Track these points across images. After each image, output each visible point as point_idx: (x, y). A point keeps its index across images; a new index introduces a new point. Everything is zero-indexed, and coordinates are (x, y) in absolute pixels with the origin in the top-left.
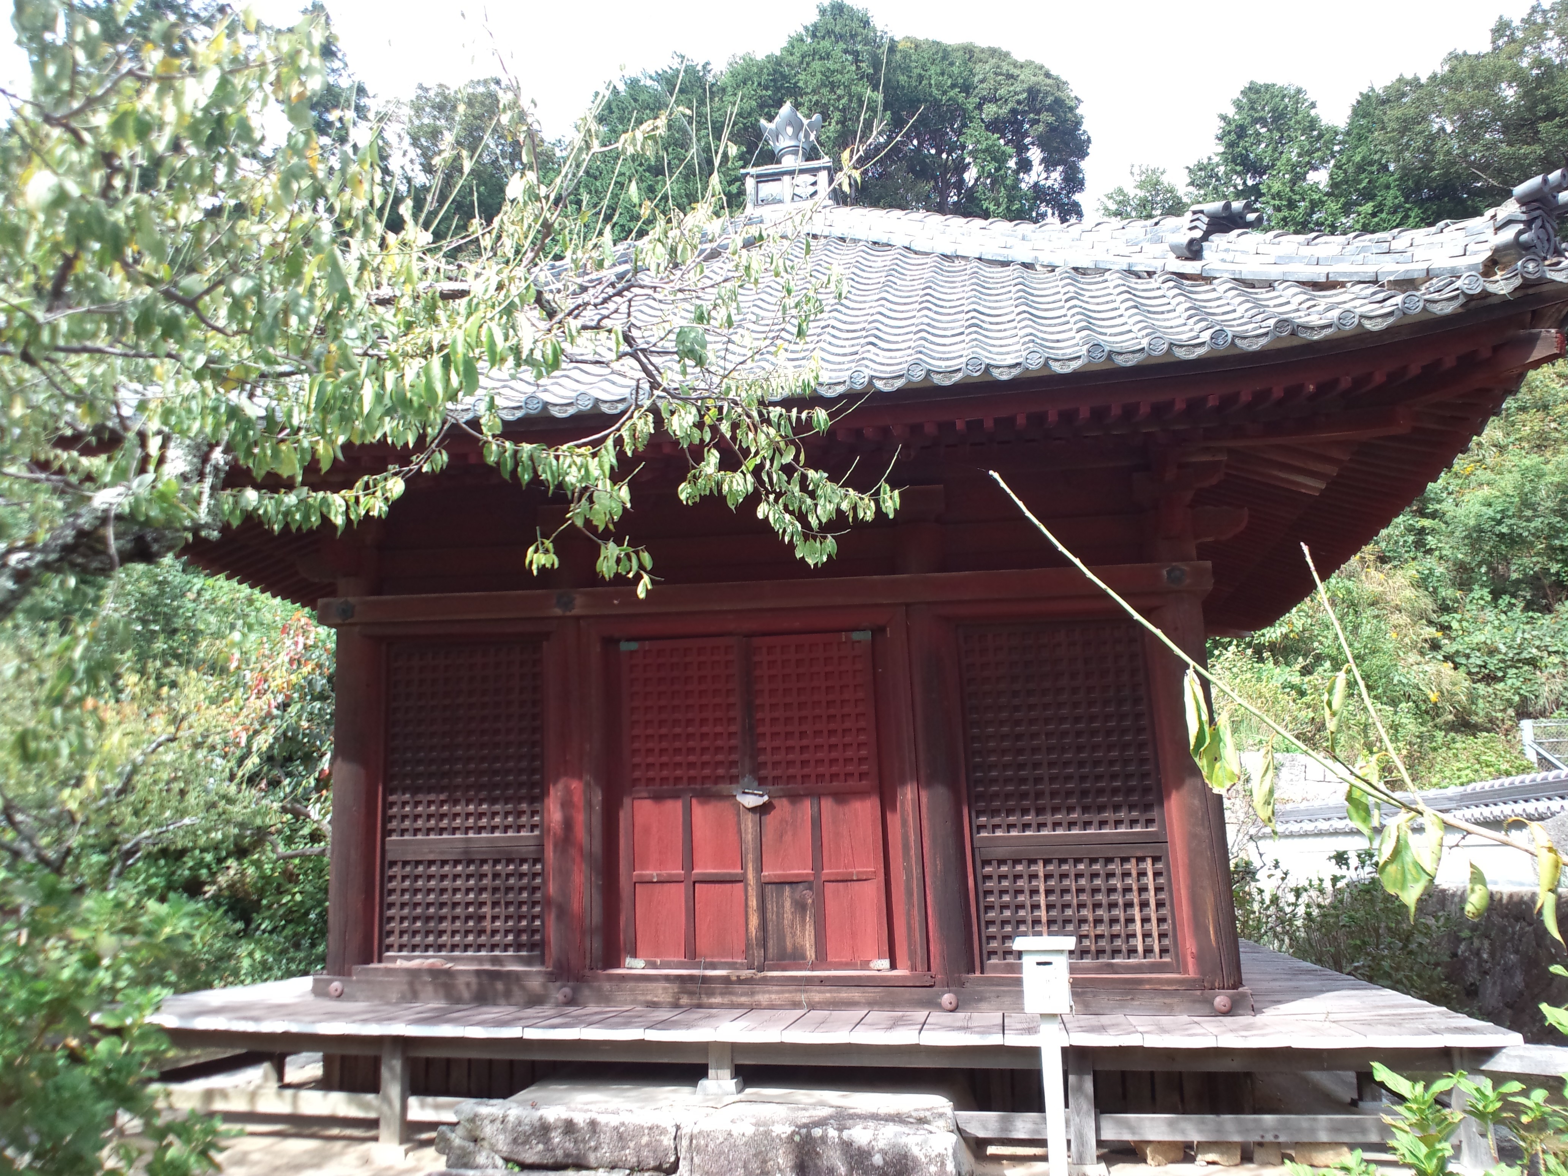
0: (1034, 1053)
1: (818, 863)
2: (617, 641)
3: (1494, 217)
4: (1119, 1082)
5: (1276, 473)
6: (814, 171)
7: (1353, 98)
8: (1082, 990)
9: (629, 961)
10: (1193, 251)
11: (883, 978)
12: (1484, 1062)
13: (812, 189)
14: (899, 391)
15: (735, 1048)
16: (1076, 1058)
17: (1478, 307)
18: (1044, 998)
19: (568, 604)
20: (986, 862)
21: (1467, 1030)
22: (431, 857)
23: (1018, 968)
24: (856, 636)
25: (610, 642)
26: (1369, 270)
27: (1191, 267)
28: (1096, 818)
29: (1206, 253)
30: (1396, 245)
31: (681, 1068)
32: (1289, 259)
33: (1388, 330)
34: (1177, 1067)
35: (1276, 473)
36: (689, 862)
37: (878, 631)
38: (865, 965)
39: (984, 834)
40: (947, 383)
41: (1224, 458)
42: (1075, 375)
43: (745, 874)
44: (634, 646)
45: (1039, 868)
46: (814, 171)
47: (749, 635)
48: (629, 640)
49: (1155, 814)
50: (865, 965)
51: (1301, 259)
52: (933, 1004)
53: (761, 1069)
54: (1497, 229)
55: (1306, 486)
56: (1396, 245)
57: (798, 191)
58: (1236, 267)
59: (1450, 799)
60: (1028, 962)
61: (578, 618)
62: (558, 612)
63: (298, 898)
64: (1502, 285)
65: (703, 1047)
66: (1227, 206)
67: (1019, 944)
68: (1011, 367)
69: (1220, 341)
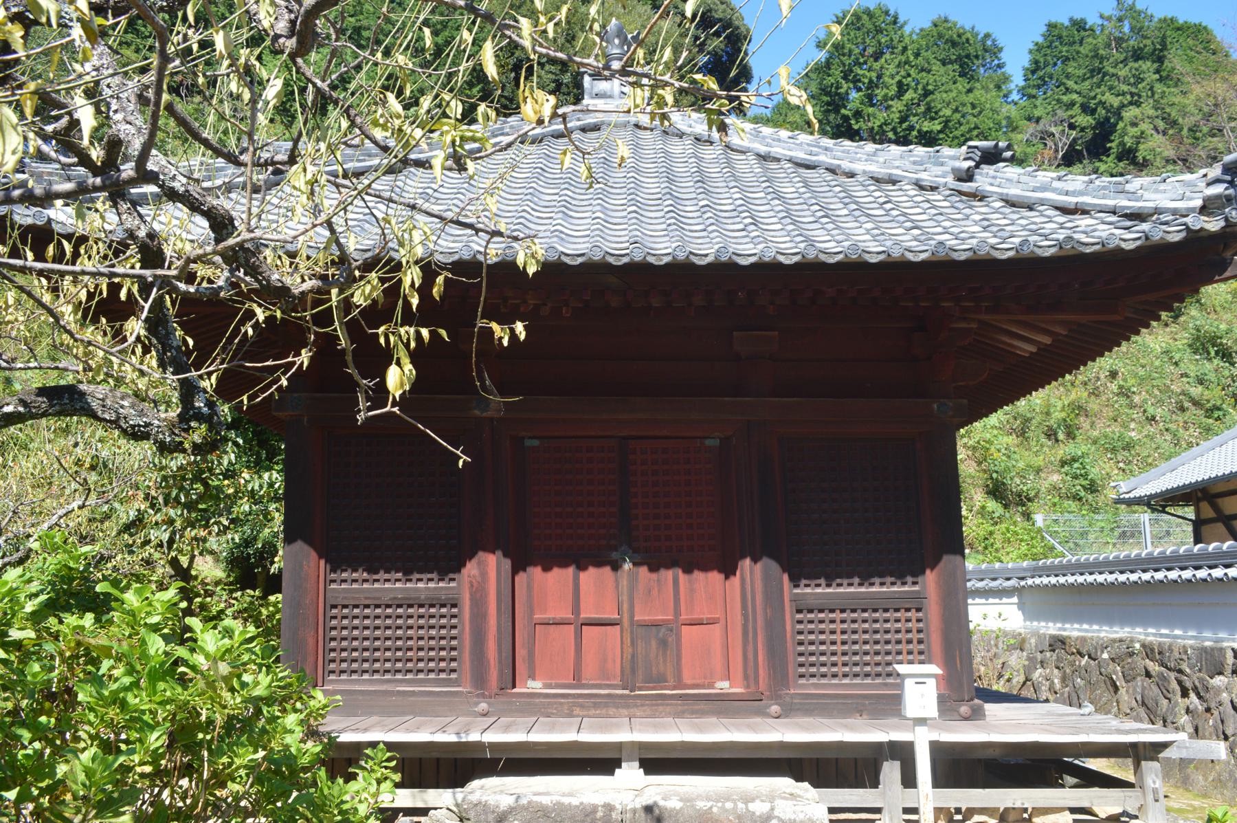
1: (677, 612)
3: (1205, 176)
4: (959, 767)
8: (947, 705)
9: (531, 683)
10: (968, 176)
11: (728, 694)
12: (1160, 752)
14: (796, 264)
16: (938, 749)
17: (1195, 238)
18: (920, 709)
20: (334, 607)
22: (367, 602)
23: (900, 686)
24: (708, 442)
26: (1110, 203)
27: (966, 187)
28: (813, 583)
29: (977, 177)
30: (1128, 187)
31: (600, 762)
32: (1044, 188)
33: (1138, 248)
36: (576, 609)
38: (711, 686)
39: (333, 586)
40: (831, 261)
41: (974, 326)
42: (923, 263)
43: (621, 619)
44: (536, 443)
47: (624, 438)
49: (920, 579)
50: (711, 686)
51: (1054, 190)
52: (763, 713)
53: (659, 762)
54: (1209, 184)
55: (1020, 349)
56: (1128, 187)
58: (1005, 191)
59: (1025, 570)
60: (909, 684)
62: (477, 412)
64: (1214, 225)
65: (619, 746)
66: (997, 145)
67: (902, 669)
68: (879, 253)
69: (1025, 248)
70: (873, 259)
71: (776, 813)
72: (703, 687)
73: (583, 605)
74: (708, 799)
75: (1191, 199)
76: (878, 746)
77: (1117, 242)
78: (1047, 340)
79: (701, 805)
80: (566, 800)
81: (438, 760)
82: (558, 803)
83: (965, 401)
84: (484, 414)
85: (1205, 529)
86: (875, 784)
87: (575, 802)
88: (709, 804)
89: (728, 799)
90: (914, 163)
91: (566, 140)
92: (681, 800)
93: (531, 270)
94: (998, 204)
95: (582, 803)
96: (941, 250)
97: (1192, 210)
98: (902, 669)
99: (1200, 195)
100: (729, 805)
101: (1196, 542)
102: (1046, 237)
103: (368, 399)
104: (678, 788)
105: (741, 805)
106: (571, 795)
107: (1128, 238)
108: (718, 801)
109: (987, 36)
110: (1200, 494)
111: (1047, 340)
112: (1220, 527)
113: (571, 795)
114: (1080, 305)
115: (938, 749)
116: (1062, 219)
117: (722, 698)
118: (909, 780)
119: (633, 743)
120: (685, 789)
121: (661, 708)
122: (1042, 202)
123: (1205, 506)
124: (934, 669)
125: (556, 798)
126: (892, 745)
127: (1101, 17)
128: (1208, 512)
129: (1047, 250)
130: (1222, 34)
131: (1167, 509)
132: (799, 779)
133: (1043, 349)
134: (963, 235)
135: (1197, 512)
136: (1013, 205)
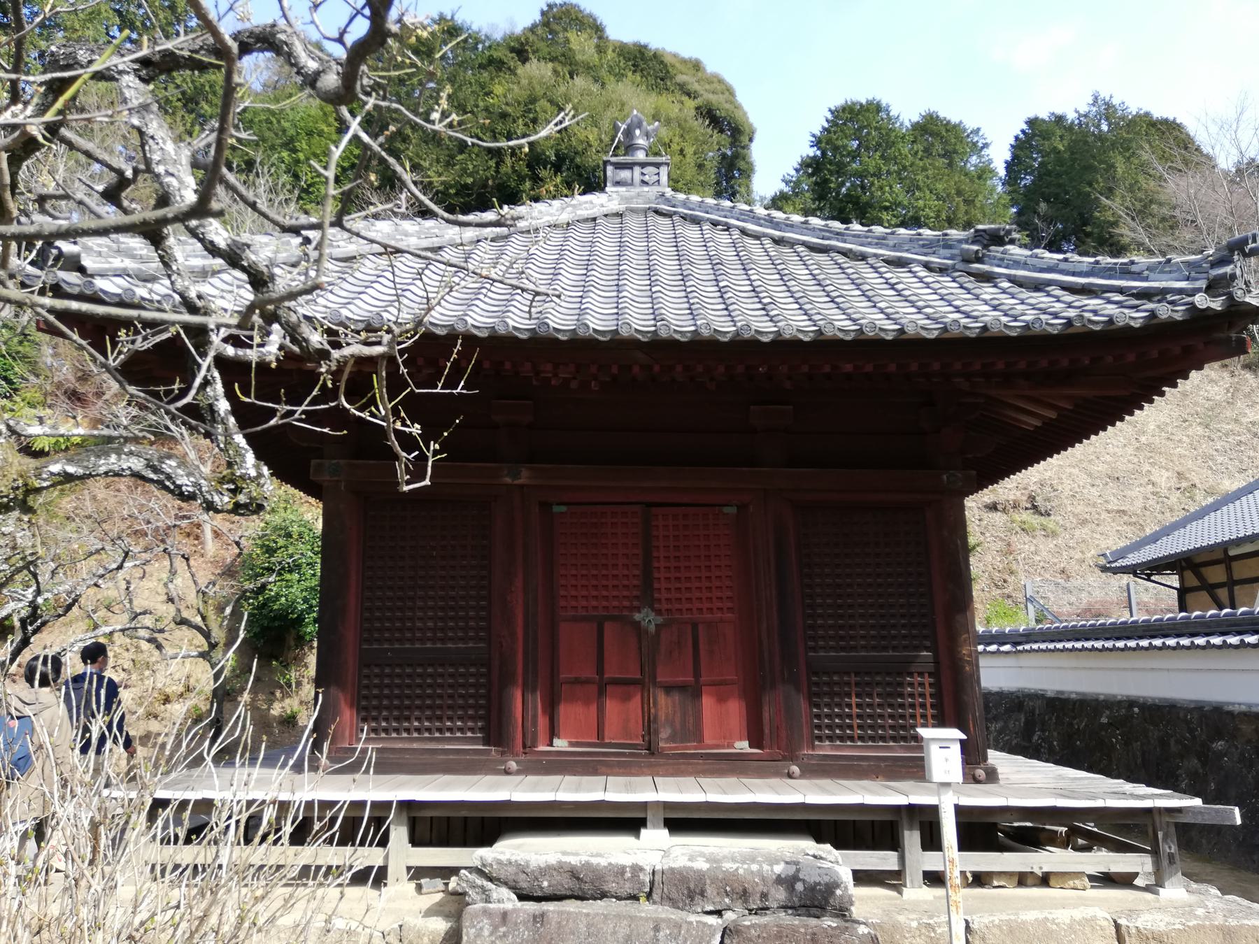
0: (934, 809)
1: (697, 674)
2: (551, 505)
5: (1014, 415)
6: (657, 165)
7: (861, 96)
13: (656, 178)
15: (667, 806)
16: (960, 810)
19: (516, 475)
21: (1161, 796)
23: (921, 748)
24: (726, 510)
25: (545, 506)
31: (626, 821)
34: (974, 820)
35: (1014, 415)
36: (600, 670)
37: (742, 507)
44: (563, 509)
45: (853, 679)
46: (657, 165)
48: (558, 504)
50: (731, 746)
53: (683, 822)
57: (646, 178)
61: (522, 486)
62: (508, 480)
63: (1055, 734)
65: (644, 806)
67: (924, 732)
70: (765, 339)
71: (801, 876)
72: (723, 747)
73: (607, 667)
74: (734, 860)
75: (1197, 279)
76: (897, 809)
77: (794, 332)
78: (1052, 415)
79: (729, 866)
80: (594, 861)
81: (466, 818)
82: (588, 864)
83: (974, 473)
84: (516, 482)
85: (1190, 598)
86: (962, 847)
87: (603, 862)
88: (735, 866)
89: (753, 860)
90: (923, 246)
91: (696, 228)
92: (708, 861)
93: (274, 365)
94: (1006, 285)
95: (610, 864)
96: (1037, 325)
97: (1199, 290)
98: (924, 732)
99: (1205, 275)
100: (755, 867)
101: (1181, 610)
102: (1056, 315)
103: (408, 471)
104: (703, 849)
105: (766, 867)
106: (598, 855)
107: (1135, 317)
108: (744, 863)
109: (977, 131)
110: (1184, 564)
111: (1052, 415)
112: (1204, 596)
113: (598, 855)
114: (1093, 379)
115: (960, 810)
116: (1069, 298)
117: (741, 757)
118: (932, 841)
119: (658, 802)
120: (711, 850)
121: (683, 767)
122: (1050, 283)
123: (1189, 574)
124: (957, 734)
125: (584, 858)
126: (911, 808)
127: (1077, 111)
128: (1192, 581)
129: (1055, 325)
130: (1193, 127)
131: (1153, 578)
132: (819, 840)
133: (1048, 423)
134: (975, 314)
135: (1182, 580)
136: (1021, 286)
